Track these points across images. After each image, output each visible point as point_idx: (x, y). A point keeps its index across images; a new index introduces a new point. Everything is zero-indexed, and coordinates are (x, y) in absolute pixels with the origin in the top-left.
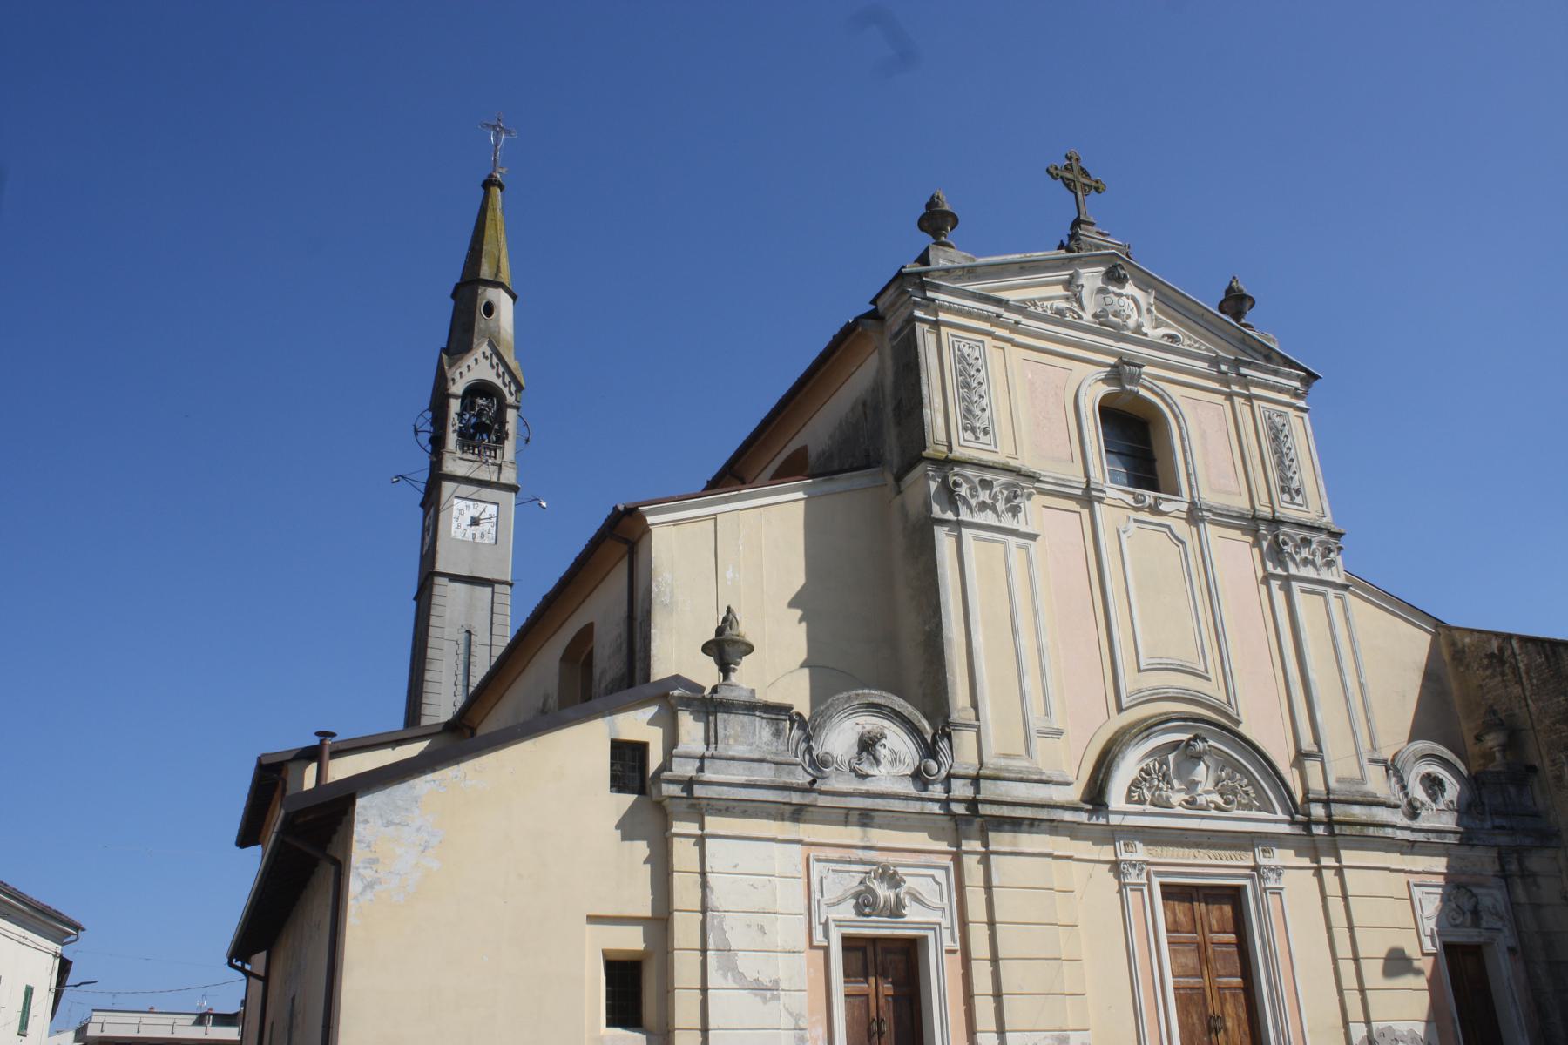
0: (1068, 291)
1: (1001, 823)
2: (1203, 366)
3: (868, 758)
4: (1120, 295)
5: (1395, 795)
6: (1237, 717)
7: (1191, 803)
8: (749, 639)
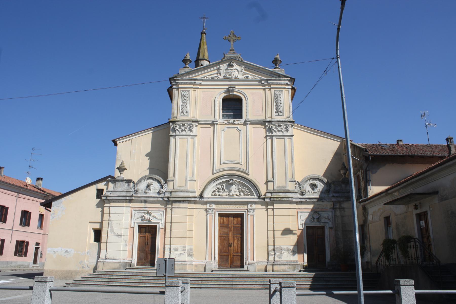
1: (175, 202)
2: (257, 83)
4: (231, 70)
8: (126, 167)
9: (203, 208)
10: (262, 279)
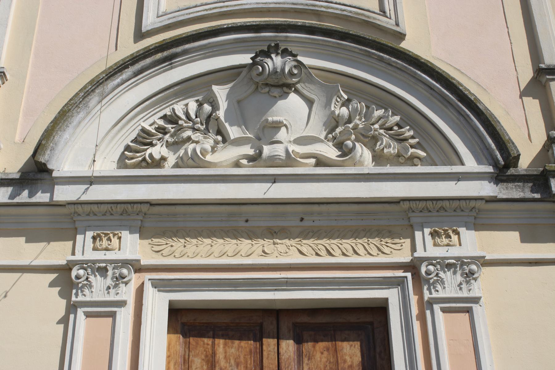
6: (398, 29)
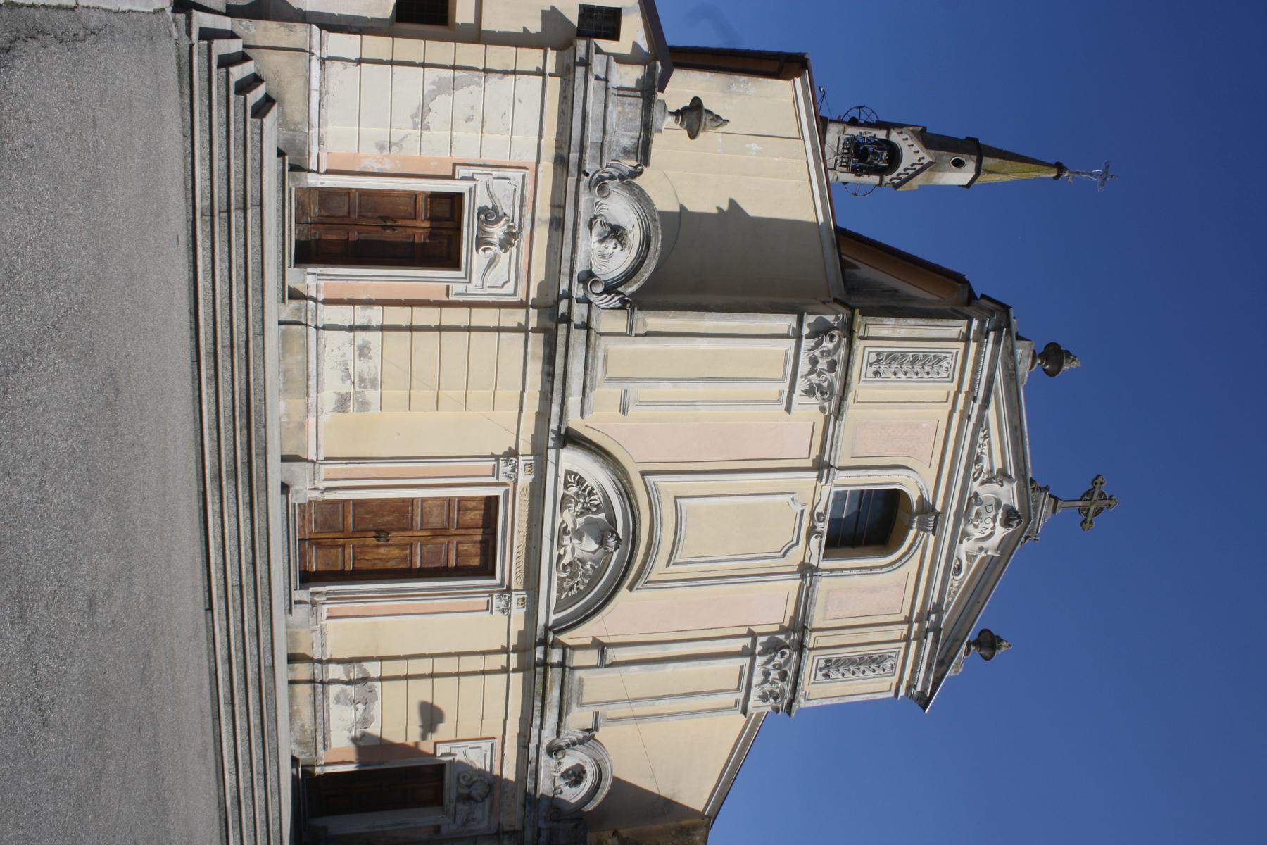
0: (997, 473)
1: (550, 345)
3: (605, 232)
4: (994, 520)
5: (568, 735)
6: (635, 588)
7: (564, 531)
8: (702, 136)
9: (521, 441)
10: (258, 770)
